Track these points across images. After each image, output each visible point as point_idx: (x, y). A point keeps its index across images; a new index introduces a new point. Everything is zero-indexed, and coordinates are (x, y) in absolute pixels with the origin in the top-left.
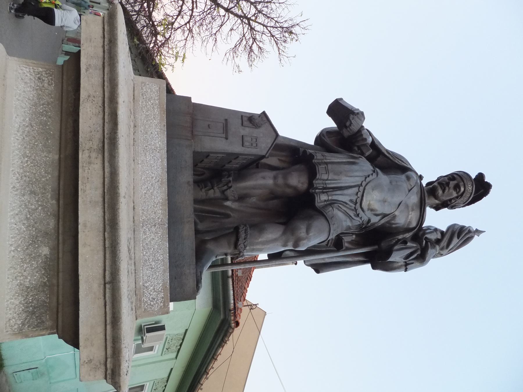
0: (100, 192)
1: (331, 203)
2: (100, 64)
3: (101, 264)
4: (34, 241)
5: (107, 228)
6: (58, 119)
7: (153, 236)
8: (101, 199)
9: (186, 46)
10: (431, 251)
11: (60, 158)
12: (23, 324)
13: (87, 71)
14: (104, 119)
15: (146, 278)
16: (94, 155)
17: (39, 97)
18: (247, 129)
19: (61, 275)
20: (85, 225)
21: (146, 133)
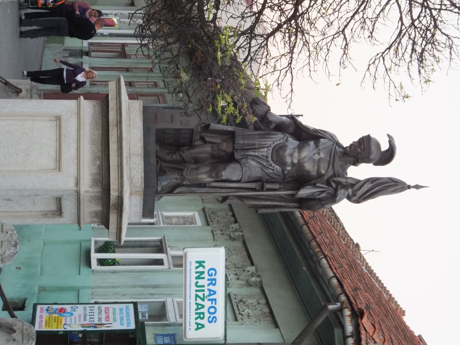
0: (116, 139)
1: (246, 157)
2: (115, 97)
4: (94, 160)
5: (119, 149)
6: (101, 119)
8: (117, 141)
9: (292, 66)
10: (341, 192)
11: (102, 133)
12: (92, 185)
15: (134, 174)
16: (114, 127)
17: (95, 113)
18: (184, 118)
19: (103, 170)
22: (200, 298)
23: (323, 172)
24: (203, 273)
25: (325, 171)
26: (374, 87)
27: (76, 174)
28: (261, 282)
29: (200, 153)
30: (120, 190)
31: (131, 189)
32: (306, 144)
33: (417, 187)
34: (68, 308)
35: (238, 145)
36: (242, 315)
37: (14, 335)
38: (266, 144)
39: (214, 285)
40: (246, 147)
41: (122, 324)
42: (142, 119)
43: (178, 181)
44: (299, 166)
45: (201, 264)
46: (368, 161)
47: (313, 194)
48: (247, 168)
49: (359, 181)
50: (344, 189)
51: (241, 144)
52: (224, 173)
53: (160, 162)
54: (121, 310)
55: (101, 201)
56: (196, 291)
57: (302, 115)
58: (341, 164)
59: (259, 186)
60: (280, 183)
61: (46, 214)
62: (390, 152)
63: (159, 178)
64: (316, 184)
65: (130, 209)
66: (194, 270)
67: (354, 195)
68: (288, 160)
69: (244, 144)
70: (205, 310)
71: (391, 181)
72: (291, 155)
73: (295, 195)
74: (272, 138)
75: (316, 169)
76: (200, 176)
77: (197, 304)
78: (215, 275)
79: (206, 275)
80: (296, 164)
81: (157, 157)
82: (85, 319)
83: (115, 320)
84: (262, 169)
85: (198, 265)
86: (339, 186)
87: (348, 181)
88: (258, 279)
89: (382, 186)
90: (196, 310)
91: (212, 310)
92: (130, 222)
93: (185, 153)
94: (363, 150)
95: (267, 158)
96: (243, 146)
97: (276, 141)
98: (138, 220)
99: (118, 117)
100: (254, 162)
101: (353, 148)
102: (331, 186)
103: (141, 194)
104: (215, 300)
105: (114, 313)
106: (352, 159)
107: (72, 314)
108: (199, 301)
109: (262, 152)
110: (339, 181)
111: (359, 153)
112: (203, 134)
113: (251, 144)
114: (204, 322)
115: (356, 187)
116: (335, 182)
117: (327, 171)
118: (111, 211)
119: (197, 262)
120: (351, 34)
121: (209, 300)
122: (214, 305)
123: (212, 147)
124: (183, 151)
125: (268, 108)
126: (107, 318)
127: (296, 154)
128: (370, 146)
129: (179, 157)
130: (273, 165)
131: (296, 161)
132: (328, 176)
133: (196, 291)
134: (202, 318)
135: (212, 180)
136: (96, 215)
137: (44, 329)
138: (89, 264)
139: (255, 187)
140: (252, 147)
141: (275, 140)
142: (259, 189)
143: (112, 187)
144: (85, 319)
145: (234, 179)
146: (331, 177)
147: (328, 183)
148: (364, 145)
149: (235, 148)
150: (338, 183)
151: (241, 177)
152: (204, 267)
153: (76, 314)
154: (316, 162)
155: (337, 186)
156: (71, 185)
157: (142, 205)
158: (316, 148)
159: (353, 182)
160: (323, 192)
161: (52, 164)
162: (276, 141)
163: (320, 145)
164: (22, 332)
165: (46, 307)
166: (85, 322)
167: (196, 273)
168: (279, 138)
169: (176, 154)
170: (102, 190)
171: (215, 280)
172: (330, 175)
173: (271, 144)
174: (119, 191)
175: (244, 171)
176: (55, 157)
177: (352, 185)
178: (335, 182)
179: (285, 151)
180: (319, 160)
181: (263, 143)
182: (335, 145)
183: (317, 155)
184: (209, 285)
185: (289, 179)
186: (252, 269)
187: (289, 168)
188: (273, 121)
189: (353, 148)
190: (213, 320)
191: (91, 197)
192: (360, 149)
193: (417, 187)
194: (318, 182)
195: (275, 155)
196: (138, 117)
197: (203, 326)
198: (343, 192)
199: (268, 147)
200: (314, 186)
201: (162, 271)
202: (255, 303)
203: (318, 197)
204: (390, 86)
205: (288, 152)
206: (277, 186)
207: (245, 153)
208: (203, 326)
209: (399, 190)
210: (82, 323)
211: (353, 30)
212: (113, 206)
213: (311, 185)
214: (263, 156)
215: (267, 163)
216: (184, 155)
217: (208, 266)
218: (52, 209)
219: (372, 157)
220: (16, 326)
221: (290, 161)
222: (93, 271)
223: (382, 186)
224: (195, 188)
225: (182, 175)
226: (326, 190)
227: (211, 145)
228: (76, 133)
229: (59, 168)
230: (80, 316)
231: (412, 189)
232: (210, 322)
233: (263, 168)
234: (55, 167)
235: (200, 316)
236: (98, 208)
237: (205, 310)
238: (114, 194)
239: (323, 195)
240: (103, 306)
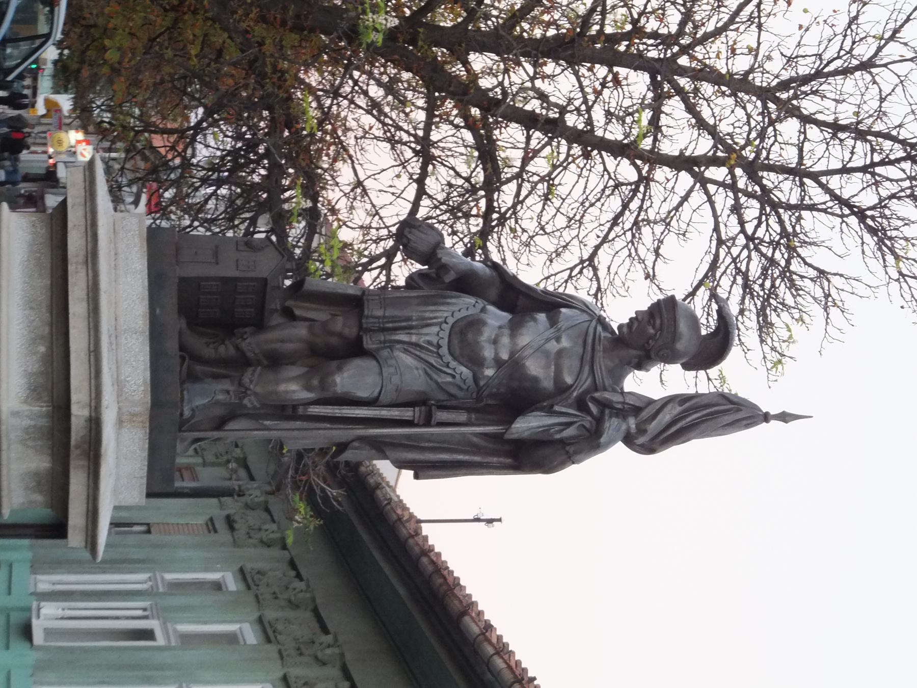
1: (391, 345)
2: (83, 201)
3: (87, 341)
4: (34, 342)
7: (134, 341)
8: (86, 297)
10: (612, 425)
12: (27, 397)
13: (72, 208)
14: (87, 240)
15: (127, 374)
20: (74, 314)
21: (127, 259)
23: (569, 380)
25: (574, 377)
26: (661, 381)
29: (282, 341)
30: (93, 404)
31: (119, 408)
32: (528, 319)
33: (785, 417)
35: (372, 320)
38: (435, 318)
40: (390, 325)
42: (146, 254)
43: (231, 398)
46: (669, 359)
48: (392, 370)
49: (651, 402)
50: (617, 416)
51: (378, 318)
52: (338, 379)
53: (187, 360)
55: (50, 452)
57: (500, 520)
58: (610, 364)
59: (420, 417)
60: (469, 410)
62: (721, 336)
63: (187, 385)
64: (552, 406)
65: (117, 466)
67: (641, 431)
68: (488, 353)
69: (384, 317)
71: (722, 401)
72: (495, 342)
73: (503, 434)
74: (448, 304)
75: (553, 374)
76: (282, 387)
80: (506, 361)
81: (182, 348)
84: (426, 373)
86: (607, 411)
87: (627, 401)
89: (705, 412)
92: (117, 504)
93: (248, 341)
94: (661, 329)
95: (438, 349)
96: (383, 323)
97: (459, 311)
98: (137, 501)
99: (91, 324)
100: (408, 357)
101: (636, 325)
102: (588, 412)
103: (142, 422)
106: (633, 352)
109: (427, 334)
110: (607, 399)
111: (652, 337)
112: (289, 303)
113: (400, 317)
115: (645, 414)
116: (596, 401)
117: (578, 376)
120: (608, 277)
123: (310, 328)
124: (242, 337)
125: (439, 238)
127: (505, 340)
128: (675, 320)
129: (232, 351)
130: (453, 364)
131: (505, 356)
132: (581, 390)
135: (310, 395)
136: (39, 483)
139: (411, 419)
140: (404, 324)
141: (457, 309)
142: (421, 423)
143: (74, 398)
145: (363, 394)
146: (586, 392)
147: (581, 405)
148: (661, 318)
149: (365, 326)
150: (604, 405)
151: (378, 390)
154: (552, 356)
155: (602, 413)
157: (146, 454)
158: (552, 326)
159: (638, 404)
162: (459, 311)
163: (560, 320)
169: (227, 342)
170: (51, 408)
172: (585, 387)
173: (446, 318)
174: (90, 406)
175: (385, 374)
177: (636, 410)
178: (596, 401)
179: (480, 332)
180: (560, 353)
181: (428, 315)
182: (594, 323)
183: (554, 342)
185: (490, 402)
187: (489, 372)
188: (451, 265)
189: (636, 325)
191: (26, 430)
192: (654, 328)
193: (785, 417)
194: (557, 404)
195: (456, 342)
196: (136, 249)
198: (616, 423)
199: (440, 324)
200: (550, 411)
203: (558, 436)
204: (697, 377)
205: (487, 334)
206: (462, 417)
207: (388, 337)
209: (745, 422)
211: (613, 270)
212: (77, 447)
213: (542, 409)
214: (429, 343)
215: (439, 360)
216: (244, 345)
219: (680, 346)
221: (493, 355)
223: (705, 412)
224: (270, 420)
225: (240, 384)
226: (575, 420)
227: (307, 323)
231: (773, 422)
233: (428, 369)
236: (42, 463)
238: (79, 412)
239: (570, 432)
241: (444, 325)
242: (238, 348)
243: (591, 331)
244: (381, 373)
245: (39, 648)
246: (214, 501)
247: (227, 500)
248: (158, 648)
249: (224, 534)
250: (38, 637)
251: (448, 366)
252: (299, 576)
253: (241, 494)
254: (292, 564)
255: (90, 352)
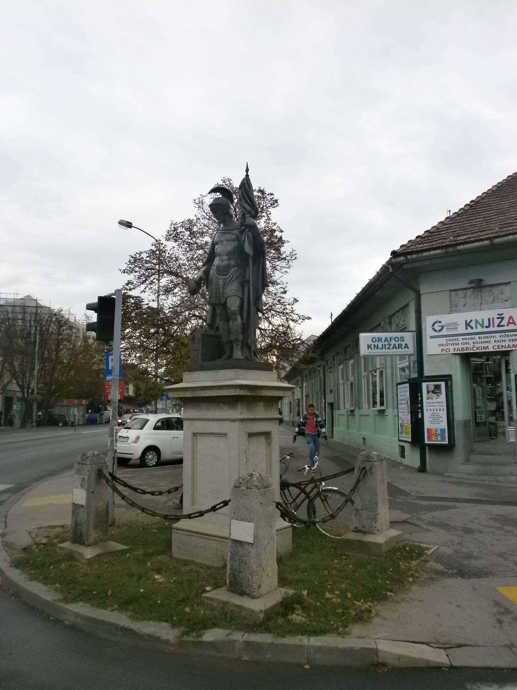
1: (223, 294)
2: (177, 392)
22: (389, 346)
23: (234, 237)
24: (374, 345)
27: (229, 422)
28: (388, 317)
33: (247, 170)
34: (400, 422)
36: (404, 325)
37: (367, 468)
39: (381, 339)
40: (218, 295)
41: (407, 391)
44: (230, 254)
45: (369, 347)
47: (249, 242)
51: (216, 299)
54: (401, 392)
56: (385, 349)
60: (245, 269)
61: (269, 444)
66: (373, 351)
68: (225, 262)
70: (397, 344)
77: (393, 348)
78: (375, 338)
79: (376, 344)
82: (405, 412)
83: (405, 395)
85: (370, 348)
88: (387, 318)
90: (396, 349)
91: (397, 339)
104: (390, 338)
105: (402, 396)
107: (403, 420)
108: (391, 347)
114: (403, 344)
115: (245, 212)
118: (259, 395)
119: (368, 349)
121: (390, 341)
122: (393, 339)
126: (404, 400)
130: (230, 274)
133: (385, 349)
134: (402, 345)
137: (410, 436)
138: (383, 411)
143: (233, 394)
144: (405, 412)
147: (242, 232)
150: (242, 225)
152: (371, 345)
153: (403, 417)
156: (236, 425)
160: (248, 236)
161: (223, 440)
164: (365, 461)
165: (400, 434)
166: (407, 412)
167: (374, 349)
168: (213, 272)
171: (378, 338)
176: (218, 438)
184: (382, 342)
186: (382, 323)
187: (232, 262)
190: (402, 339)
193: (247, 170)
197: (406, 344)
200: (244, 241)
201: (386, 371)
202: (398, 318)
203: (252, 239)
206: (247, 270)
208: (406, 344)
210: (407, 414)
214: (223, 282)
217: (370, 343)
218: (264, 440)
220: (360, 467)
222: (387, 408)
228: (203, 422)
229: (223, 435)
230: (404, 415)
232: (404, 340)
234: (225, 438)
235: (400, 346)
236: (261, 405)
237: (397, 344)
240: (399, 402)
241: (218, 277)
242: (227, 343)
243: (220, 232)
244: (232, 296)
245: (355, 408)
246: (326, 372)
247: (326, 369)
248: (354, 381)
249: (332, 369)
250: (353, 408)
251: (230, 276)
252: (340, 352)
253: (324, 366)
254: (338, 354)
255: (220, 389)
